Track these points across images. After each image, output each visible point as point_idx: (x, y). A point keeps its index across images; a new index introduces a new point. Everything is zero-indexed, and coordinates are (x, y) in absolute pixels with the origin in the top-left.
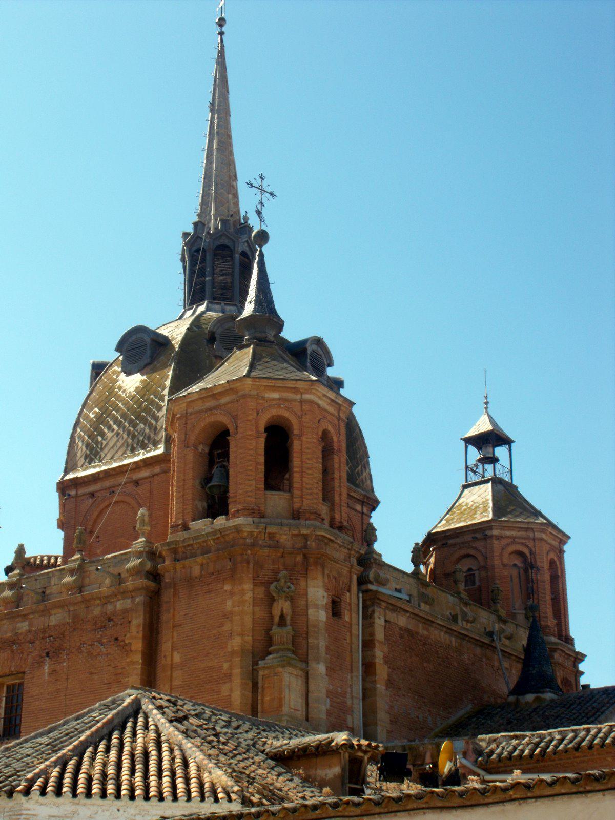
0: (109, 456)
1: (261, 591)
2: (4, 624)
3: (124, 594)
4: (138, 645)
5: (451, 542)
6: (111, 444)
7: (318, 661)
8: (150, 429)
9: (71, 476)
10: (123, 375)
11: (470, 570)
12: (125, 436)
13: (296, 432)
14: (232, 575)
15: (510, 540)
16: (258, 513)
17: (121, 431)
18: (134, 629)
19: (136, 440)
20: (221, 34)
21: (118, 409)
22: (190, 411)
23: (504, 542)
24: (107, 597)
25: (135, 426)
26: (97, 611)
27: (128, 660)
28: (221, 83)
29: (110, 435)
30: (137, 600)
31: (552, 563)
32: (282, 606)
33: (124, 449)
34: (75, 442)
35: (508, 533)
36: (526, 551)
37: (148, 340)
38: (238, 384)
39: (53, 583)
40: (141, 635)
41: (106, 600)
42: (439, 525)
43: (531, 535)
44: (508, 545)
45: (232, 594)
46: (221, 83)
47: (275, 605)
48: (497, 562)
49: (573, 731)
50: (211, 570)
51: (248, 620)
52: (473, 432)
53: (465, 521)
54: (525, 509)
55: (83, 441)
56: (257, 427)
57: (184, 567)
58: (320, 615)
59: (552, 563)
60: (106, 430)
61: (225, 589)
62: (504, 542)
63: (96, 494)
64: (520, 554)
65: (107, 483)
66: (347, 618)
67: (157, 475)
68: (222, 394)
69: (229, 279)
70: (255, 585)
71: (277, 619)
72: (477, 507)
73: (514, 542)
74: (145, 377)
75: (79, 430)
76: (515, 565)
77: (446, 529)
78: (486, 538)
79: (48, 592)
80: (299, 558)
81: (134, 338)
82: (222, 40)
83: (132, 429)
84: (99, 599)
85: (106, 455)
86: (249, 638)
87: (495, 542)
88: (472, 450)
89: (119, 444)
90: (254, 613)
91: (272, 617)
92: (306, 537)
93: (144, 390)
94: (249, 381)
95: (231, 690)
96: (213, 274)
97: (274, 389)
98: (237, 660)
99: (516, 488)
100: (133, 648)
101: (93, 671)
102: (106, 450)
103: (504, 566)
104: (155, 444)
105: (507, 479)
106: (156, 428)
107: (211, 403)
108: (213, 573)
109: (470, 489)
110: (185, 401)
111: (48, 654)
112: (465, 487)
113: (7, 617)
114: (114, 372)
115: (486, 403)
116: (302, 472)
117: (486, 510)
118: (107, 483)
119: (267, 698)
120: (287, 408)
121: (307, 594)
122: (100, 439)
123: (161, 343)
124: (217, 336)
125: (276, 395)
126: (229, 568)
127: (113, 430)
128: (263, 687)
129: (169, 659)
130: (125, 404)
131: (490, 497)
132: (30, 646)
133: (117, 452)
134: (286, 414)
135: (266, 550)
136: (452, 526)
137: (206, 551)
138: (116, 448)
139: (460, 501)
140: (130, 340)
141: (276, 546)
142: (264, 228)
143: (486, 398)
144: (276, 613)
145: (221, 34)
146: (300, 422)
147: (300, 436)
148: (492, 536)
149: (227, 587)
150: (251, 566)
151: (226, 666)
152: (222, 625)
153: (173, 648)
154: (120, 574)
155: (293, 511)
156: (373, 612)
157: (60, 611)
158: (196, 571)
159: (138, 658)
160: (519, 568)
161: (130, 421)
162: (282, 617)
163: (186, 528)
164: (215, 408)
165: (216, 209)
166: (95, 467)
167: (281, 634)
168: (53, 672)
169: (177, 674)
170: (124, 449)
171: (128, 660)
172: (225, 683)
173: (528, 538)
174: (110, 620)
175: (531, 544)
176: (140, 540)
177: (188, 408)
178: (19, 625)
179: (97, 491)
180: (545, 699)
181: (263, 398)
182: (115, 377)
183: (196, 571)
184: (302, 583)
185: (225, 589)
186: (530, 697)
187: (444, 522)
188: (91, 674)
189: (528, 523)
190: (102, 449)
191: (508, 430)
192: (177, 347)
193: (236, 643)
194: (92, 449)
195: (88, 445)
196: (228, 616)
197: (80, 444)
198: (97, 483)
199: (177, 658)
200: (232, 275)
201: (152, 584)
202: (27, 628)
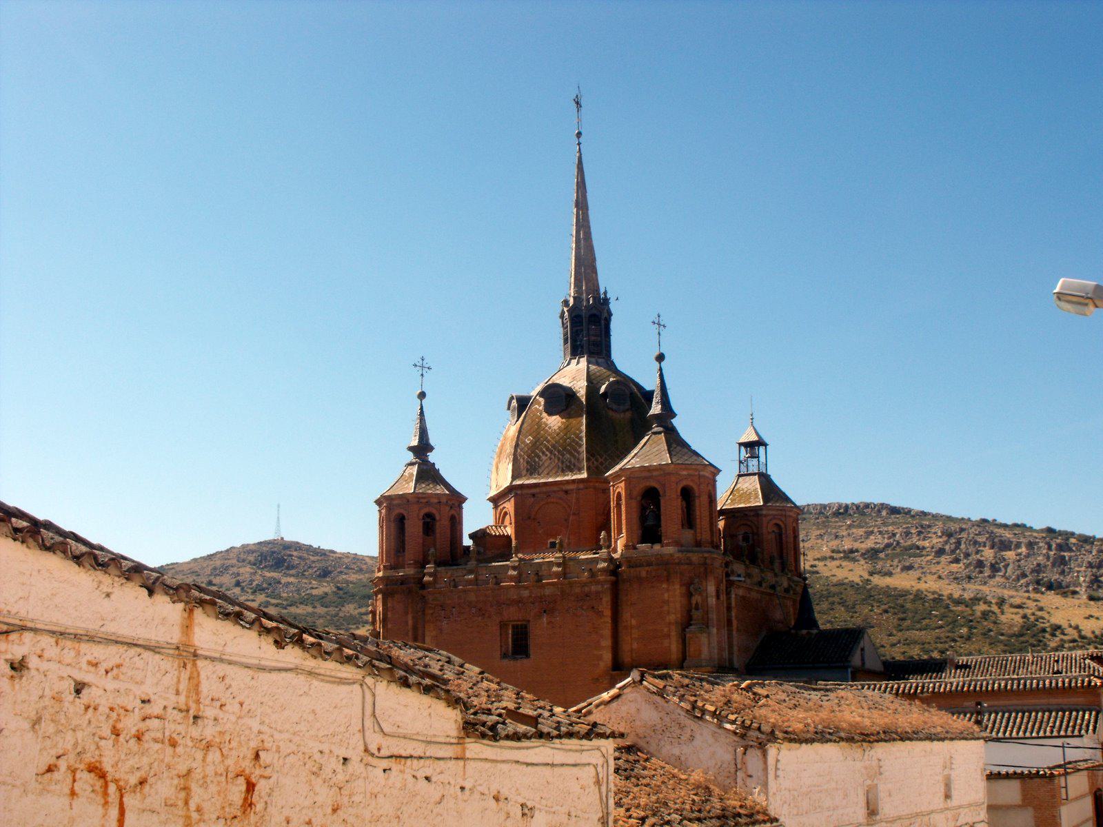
0: (545, 472)
1: (684, 589)
3: (598, 582)
4: (608, 613)
5: (736, 514)
7: (713, 627)
8: (575, 459)
10: (545, 415)
12: (556, 461)
15: (772, 517)
16: (677, 543)
21: (548, 441)
23: (769, 518)
25: (563, 455)
26: (577, 590)
27: (602, 621)
28: (581, 186)
29: (544, 458)
32: (696, 599)
33: (556, 469)
35: (771, 512)
39: (543, 568)
40: (610, 607)
41: (584, 585)
42: (727, 503)
43: (784, 513)
46: (581, 186)
47: (693, 598)
48: (764, 531)
50: (654, 574)
51: (678, 605)
52: (742, 441)
53: (744, 502)
54: (779, 495)
56: (677, 492)
58: (712, 601)
60: (541, 454)
61: (663, 586)
62: (769, 518)
63: (536, 495)
65: (544, 489)
66: (722, 599)
69: (599, 339)
70: (681, 586)
71: (694, 606)
72: (750, 493)
73: (775, 518)
75: (519, 450)
76: (773, 531)
79: (540, 574)
80: (702, 570)
82: (580, 149)
83: (561, 457)
86: (679, 616)
87: (764, 518)
88: (743, 449)
89: (552, 466)
90: (681, 602)
92: (706, 558)
93: (566, 429)
94: (673, 466)
95: (670, 643)
96: (588, 335)
97: (686, 469)
98: (673, 628)
100: (605, 614)
102: (543, 468)
103: (769, 532)
105: (764, 472)
107: (647, 474)
112: (740, 476)
116: (701, 518)
117: (757, 497)
118: (544, 489)
120: (692, 480)
121: (707, 590)
122: (537, 460)
124: (609, 394)
127: (546, 455)
128: (689, 644)
129: (629, 622)
130: (553, 438)
132: (532, 605)
133: (551, 470)
134: (691, 484)
135: (686, 566)
136: (736, 506)
137: (649, 564)
139: (738, 486)
141: (690, 563)
145: (579, 144)
146: (699, 489)
147: (699, 497)
148: (762, 515)
149: (664, 586)
150: (678, 575)
151: (666, 630)
152: (662, 607)
155: (696, 541)
156: (731, 590)
157: (552, 587)
158: (644, 574)
159: (609, 620)
160: (775, 533)
161: (559, 451)
165: (586, 286)
166: (535, 478)
168: (549, 623)
170: (556, 469)
171: (602, 621)
173: (781, 515)
174: (587, 596)
175: (783, 519)
176: (603, 551)
178: (522, 592)
180: (812, 634)
181: (679, 475)
184: (704, 584)
185: (663, 586)
186: (804, 632)
188: (577, 626)
189: (783, 507)
192: (583, 400)
193: (672, 618)
195: (528, 462)
196: (667, 602)
197: (522, 460)
201: (613, 578)
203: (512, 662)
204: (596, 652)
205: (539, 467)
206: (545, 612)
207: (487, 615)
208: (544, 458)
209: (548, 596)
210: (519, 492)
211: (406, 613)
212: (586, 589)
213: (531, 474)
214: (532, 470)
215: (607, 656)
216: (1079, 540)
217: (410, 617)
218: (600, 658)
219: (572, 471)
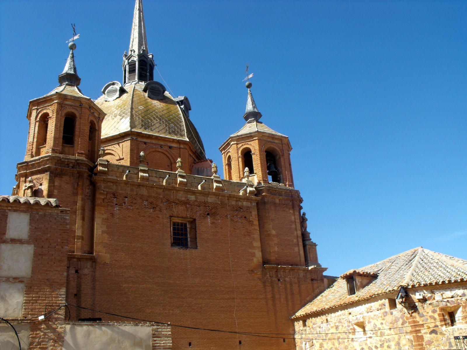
2: (180, 193)
4: (256, 223)
24: (240, 198)
26: (233, 203)
30: (253, 204)
38: (284, 139)
50: (283, 202)
57: (272, 198)
63: (148, 144)
68: (277, 139)
81: (157, 86)
84: (236, 198)
101: (235, 227)
108: (284, 204)
110: (263, 134)
113: (186, 190)
119: (311, 256)
126: (291, 204)
140: (152, 85)
157: (214, 197)
158: (277, 201)
159: (257, 228)
166: (147, 131)
168: (213, 223)
172: (295, 247)
178: (189, 196)
179: (148, 143)
188: (234, 229)
195: (142, 121)
197: (137, 119)
198: (148, 139)
203: (181, 250)
204: (250, 250)
205: (152, 126)
206: (208, 214)
207: (158, 209)
208: (155, 121)
209: (211, 203)
210: (134, 138)
211: (76, 194)
212: (240, 203)
213: (145, 129)
214: (146, 126)
215: (259, 254)
216: (32, 338)
217: (79, 198)
218: (253, 255)
219: (176, 135)
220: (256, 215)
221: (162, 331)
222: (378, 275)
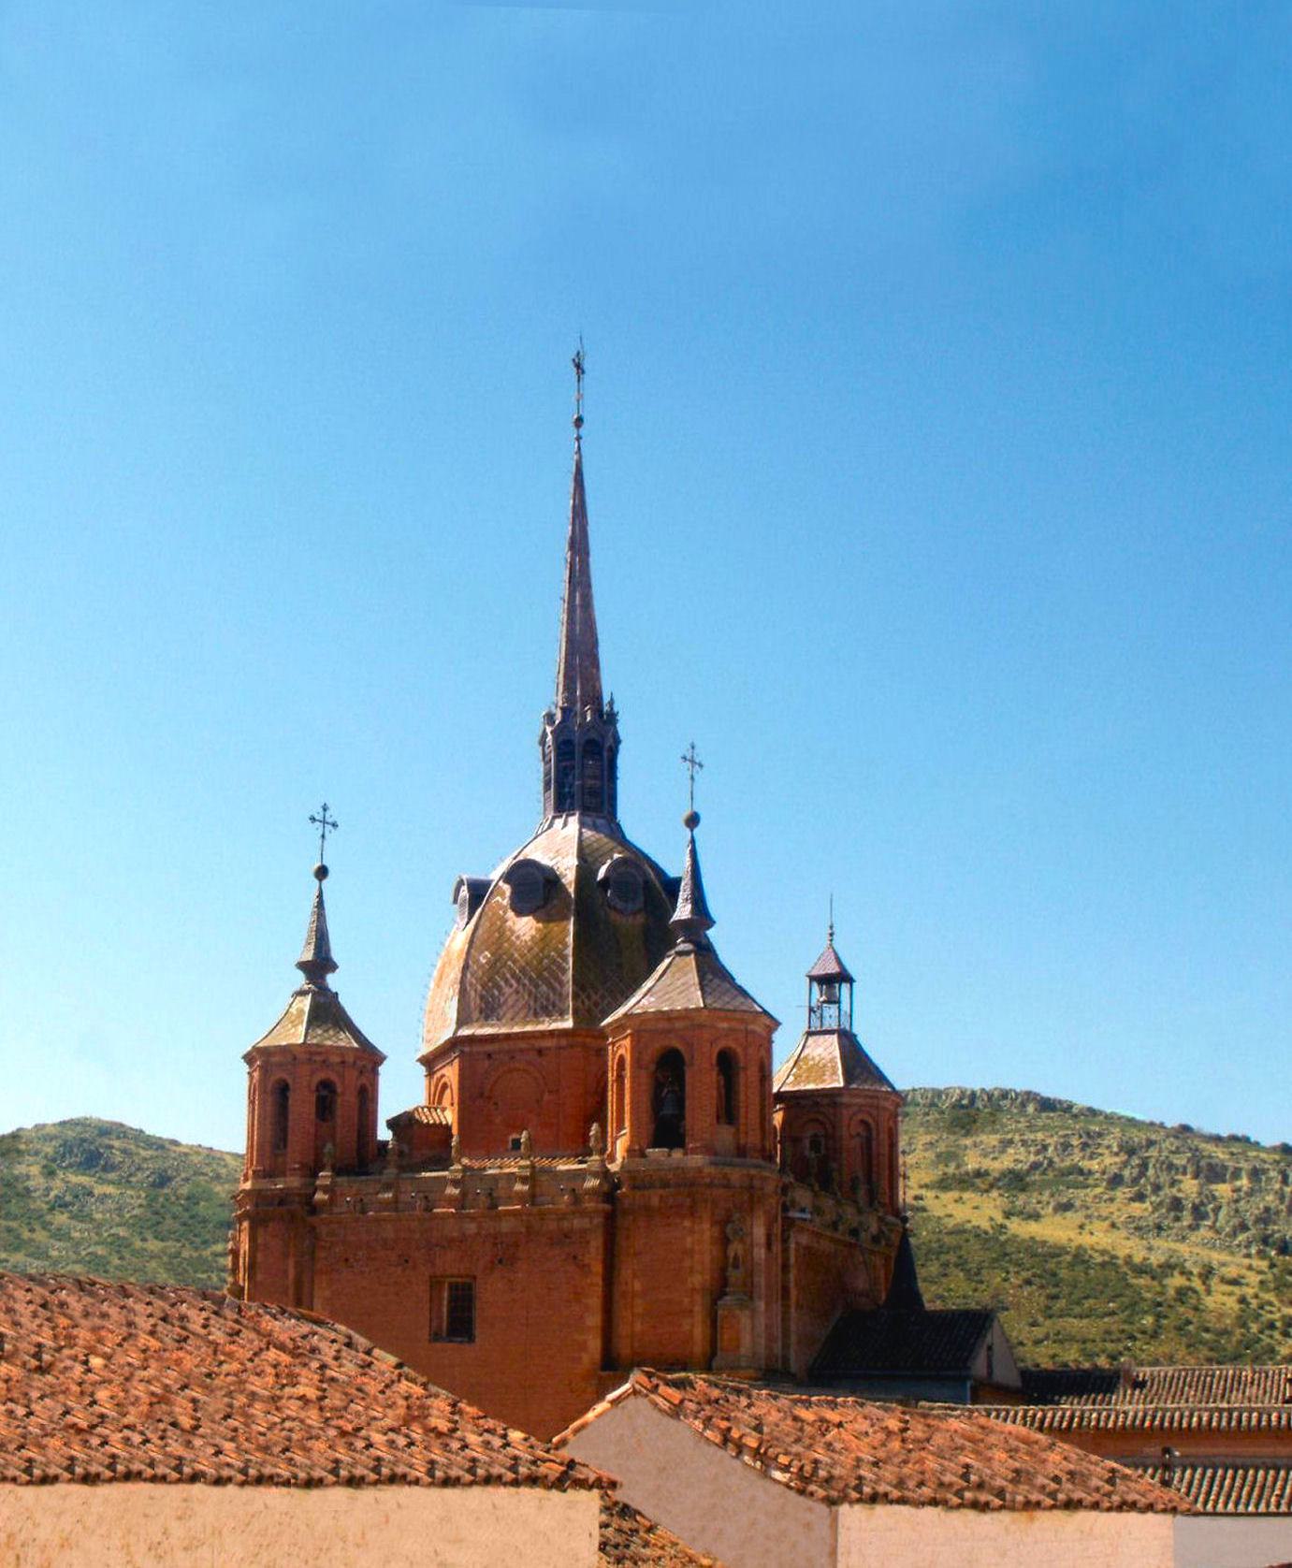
1: (716, 1230)
3: (583, 1213)
4: (598, 1268)
6: (510, 1002)
7: (760, 1298)
9: (465, 1032)
10: (511, 914)
11: (816, 1135)
12: (526, 997)
13: (742, 1065)
14: (692, 1213)
17: (521, 988)
18: (593, 1250)
19: (538, 1003)
20: (579, 438)
22: (643, 1027)
26: (553, 1226)
27: (589, 1281)
29: (507, 990)
31: (890, 1129)
32: (736, 1248)
34: (465, 990)
36: (870, 1121)
37: (541, 878)
39: (500, 1185)
40: (600, 1257)
41: (562, 1217)
44: (854, 1114)
45: (692, 1232)
48: (844, 1132)
49: (996, 1410)
50: (671, 1202)
51: (707, 1258)
55: (476, 991)
59: (890, 1129)
64: (863, 1122)
67: (563, 1048)
72: (825, 1066)
74: (540, 925)
75: (469, 976)
77: (796, 1089)
78: (835, 1105)
79: (495, 1195)
85: (504, 1014)
86: (708, 1277)
91: (726, 1256)
92: (751, 1178)
93: (543, 940)
95: (693, 1325)
98: (698, 1298)
99: (855, 1036)
101: (552, 1286)
102: (505, 1008)
104: (562, 1014)
106: (560, 995)
109: (815, 1038)
111: (500, 1261)
112: (810, 1034)
114: (500, 906)
115: (831, 935)
117: (834, 1073)
119: (726, 1337)
122: (496, 993)
123: (550, 880)
125: (725, 1025)
127: (511, 986)
131: (837, 1053)
134: (733, 1045)
136: (802, 1087)
137: (665, 1185)
138: (516, 1009)
142: (696, 809)
143: (831, 927)
144: (731, 1254)
146: (746, 1055)
148: (842, 1104)
150: (709, 1205)
153: (635, 1276)
154: (574, 1190)
158: (655, 1201)
159: (599, 1280)
161: (531, 979)
162: (736, 1257)
163: (643, 1155)
164: (669, 1031)
165: (582, 689)
166: (492, 1026)
167: (734, 1275)
169: (638, 1301)
173: (871, 1106)
174: (566, 1236)
177: (641, 1024)
178: (466, 1226)
182: (501, 912)
183: (655, 1201)
187: (791, 1078)
190: (500, 1006)
191: (852, 970)
194: (487, 1003)
195: (482, 997)
197: (473, 993)
199: (637, 1286)
200: (602, 779)
201: (607, 1207)
202: (476, 1231)
207: (410, 1264)
215: (595, 1344)
218: (583, 1347)
220: (597, 1248)
221: (933, 1409)
222: (682, 1417)
